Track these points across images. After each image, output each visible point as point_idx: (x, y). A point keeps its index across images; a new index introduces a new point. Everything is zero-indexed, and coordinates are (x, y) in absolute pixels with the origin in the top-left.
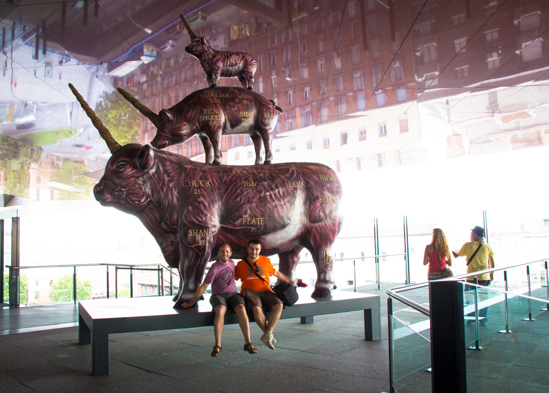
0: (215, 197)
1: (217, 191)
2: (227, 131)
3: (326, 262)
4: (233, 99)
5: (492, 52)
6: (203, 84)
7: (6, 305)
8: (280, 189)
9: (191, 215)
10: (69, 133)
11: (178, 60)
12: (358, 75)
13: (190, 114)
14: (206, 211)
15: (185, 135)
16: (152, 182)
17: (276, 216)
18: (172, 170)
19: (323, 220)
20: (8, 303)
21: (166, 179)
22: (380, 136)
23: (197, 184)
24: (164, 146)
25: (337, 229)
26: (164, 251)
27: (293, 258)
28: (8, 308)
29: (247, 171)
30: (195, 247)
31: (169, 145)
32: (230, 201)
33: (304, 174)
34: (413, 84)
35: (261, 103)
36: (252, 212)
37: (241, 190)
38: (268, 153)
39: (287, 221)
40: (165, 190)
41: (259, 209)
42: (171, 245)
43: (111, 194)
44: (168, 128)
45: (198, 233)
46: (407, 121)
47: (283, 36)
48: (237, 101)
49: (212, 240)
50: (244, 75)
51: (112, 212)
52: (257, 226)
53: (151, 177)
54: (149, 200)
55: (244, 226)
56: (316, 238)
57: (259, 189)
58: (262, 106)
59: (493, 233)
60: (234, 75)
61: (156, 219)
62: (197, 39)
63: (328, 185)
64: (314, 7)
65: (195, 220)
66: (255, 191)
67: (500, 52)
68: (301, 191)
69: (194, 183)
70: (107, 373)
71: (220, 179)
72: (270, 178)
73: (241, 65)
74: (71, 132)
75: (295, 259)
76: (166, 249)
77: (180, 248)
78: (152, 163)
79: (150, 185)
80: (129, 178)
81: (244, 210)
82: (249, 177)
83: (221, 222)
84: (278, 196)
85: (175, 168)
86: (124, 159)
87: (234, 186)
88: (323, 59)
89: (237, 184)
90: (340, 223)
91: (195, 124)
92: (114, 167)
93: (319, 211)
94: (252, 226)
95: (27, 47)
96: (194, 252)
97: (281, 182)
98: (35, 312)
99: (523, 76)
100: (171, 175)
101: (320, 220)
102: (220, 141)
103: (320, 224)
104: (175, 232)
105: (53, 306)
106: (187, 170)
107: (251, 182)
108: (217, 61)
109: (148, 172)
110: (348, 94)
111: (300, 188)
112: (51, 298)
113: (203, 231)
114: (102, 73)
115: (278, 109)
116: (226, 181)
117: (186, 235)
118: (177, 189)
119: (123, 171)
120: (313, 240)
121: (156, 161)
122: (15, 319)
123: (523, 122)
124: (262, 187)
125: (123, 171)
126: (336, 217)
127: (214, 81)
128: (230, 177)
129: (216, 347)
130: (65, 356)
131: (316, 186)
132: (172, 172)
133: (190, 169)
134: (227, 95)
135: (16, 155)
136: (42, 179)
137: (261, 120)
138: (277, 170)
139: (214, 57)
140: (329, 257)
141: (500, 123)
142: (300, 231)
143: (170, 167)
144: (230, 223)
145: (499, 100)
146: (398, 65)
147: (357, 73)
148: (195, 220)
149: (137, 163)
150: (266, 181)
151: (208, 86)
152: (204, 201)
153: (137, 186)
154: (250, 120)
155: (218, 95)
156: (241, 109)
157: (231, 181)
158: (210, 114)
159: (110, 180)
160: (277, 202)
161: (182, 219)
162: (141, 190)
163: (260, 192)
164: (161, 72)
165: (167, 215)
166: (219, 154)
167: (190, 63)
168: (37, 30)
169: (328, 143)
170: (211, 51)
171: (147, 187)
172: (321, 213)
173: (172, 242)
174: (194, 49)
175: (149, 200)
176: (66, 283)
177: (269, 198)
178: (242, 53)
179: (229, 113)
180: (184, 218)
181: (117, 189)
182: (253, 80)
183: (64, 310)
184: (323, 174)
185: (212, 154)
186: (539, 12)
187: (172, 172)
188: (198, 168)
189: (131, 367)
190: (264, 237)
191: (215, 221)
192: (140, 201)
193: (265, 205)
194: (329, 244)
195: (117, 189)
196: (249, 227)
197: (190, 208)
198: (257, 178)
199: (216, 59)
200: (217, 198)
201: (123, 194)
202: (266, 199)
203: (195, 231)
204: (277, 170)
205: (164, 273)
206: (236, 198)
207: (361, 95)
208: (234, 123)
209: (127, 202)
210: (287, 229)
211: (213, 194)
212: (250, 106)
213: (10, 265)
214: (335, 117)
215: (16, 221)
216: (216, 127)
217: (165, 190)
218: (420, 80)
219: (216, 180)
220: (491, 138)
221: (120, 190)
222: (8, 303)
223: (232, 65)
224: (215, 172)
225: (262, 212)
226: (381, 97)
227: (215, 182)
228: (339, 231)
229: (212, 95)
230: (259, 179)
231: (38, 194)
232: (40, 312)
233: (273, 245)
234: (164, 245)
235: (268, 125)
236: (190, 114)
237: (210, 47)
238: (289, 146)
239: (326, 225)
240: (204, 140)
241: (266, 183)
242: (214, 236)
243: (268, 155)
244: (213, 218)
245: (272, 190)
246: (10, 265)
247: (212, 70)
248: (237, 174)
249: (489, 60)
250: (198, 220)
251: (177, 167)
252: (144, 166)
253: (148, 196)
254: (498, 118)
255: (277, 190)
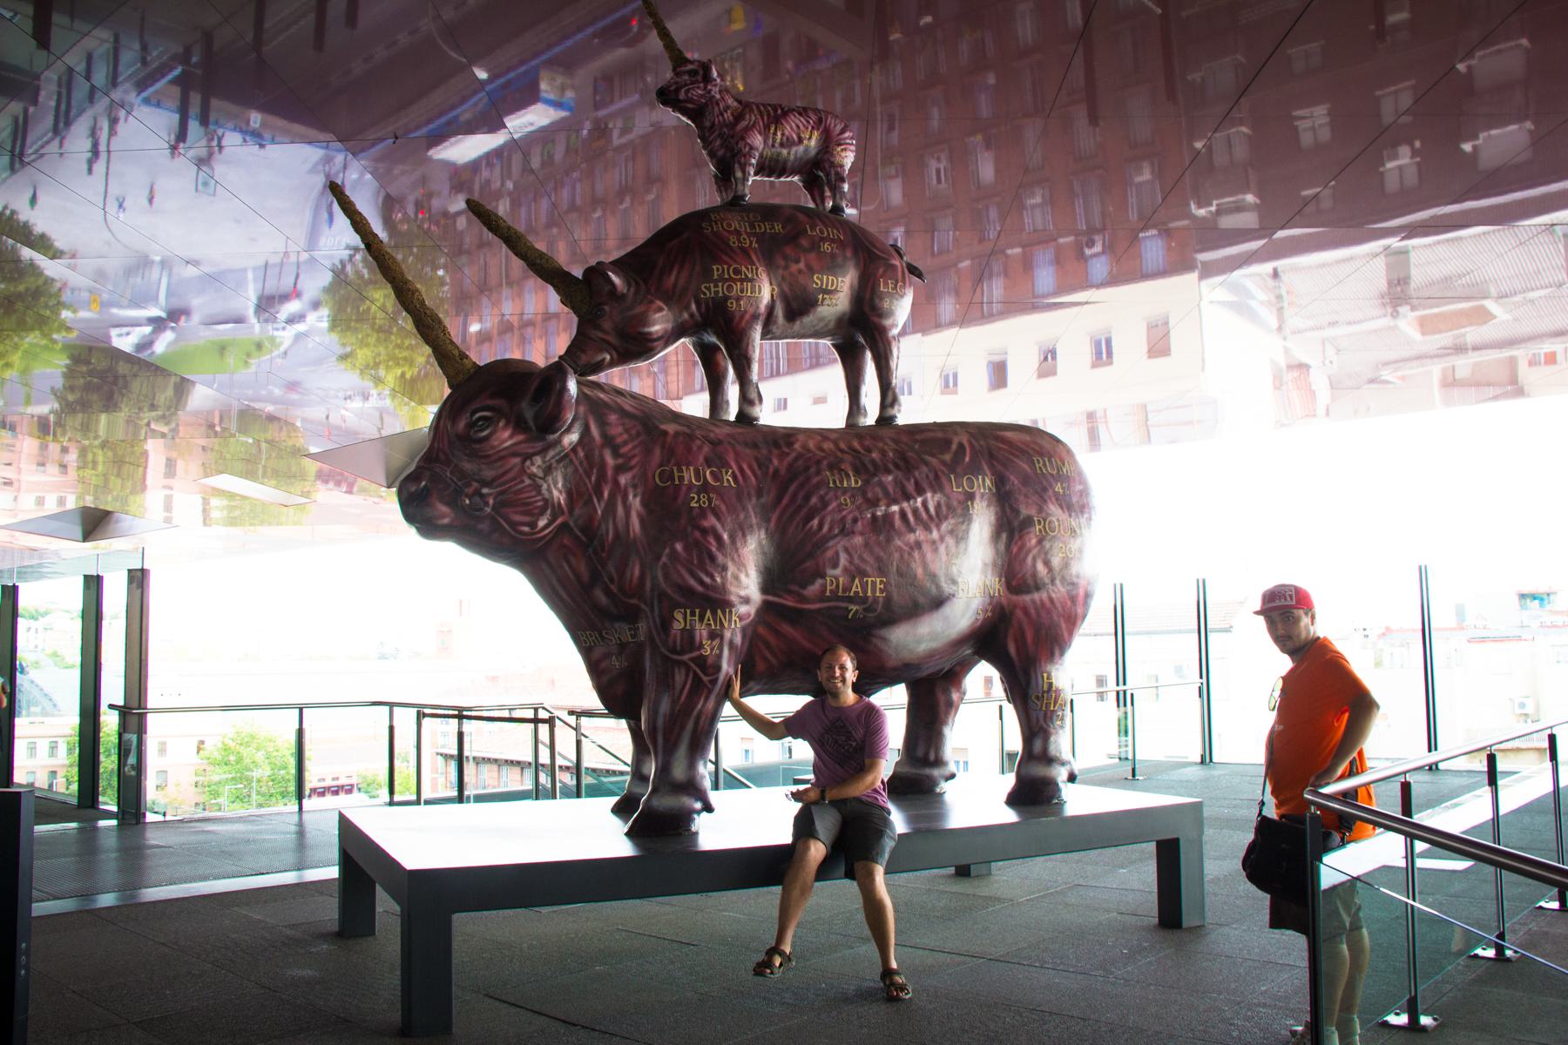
0: (747, 517)
1: (754, 500)
2: (774, 329)
3: (1048, 705)
4: (793, 238)
5: (1395, 145)
6: (706, 196)
7: (108, 815)
8: (929, 495)
9: (679, 567)
10: (253, 348)
11: (551, 156)
12: (1038, 200)
13: (673, 278)
14: (725, 555)
15: (659, 339)
16: (570, 470)
17: (919, 571)
18: (625, 436)
19: (1045, 585)
20: (115, 808)
21: (610, 461)
22: (1094, 366)
23: (698, 479)
24: (598, 367)
25: (1080, 611)
26: (594, 668)
27: (947, 692)
28: (114, 822)
29: (835, 442)
30: (692, 659)
31: (612, 364)
32: (791, 529)
33: (991, 455)
34: (1185, 223)
35: (870, 252)
36: (851, 562)
37: (822, 498)
38: (888, 396)
39: (947, 588)
40: (606, 494)
41: (872, 552)
42: (620, 654)
43: (453, 503)
44: (608, 316)
45: (702, 619)
46: (1166, 323)
47: (838, 96)
48: (804, 243)
49: (738, 640)
50: (818, 174)
51: (451, 555)
52: (864, 600)
53: (566, 456)
54: (559, 521)
55: (829, 599)
56: (1021, 639)
57: (870, 495)
58: (874, 261)
59: (1388, 629)
60: (793, 173)
61: (578, 577)
62: (690, 67)
63: (1058, 488)
64: (920, 15)
65: (692, 582)
66: (860, 501)
67: (1417, 144)
68: (985, 504)
69: (689, 475)
70: (447, 1028)
71: (760, 466)
72: (901, 464)
73: (813, 143)
74: (259, 346)
75: (955, 696)
76: (604, 665)
77: (648, 664)
78: (570, 417)
79: (565, 478)
80: (503, 458)
81: (829, 554)
82: (841, 460)
83: (766, 588)
84: (924, 515)
85: (634, 432)
86: (490, 402)
87: (802, 486)
88: (943, 157)
89: (808, 479)
90: (1088, 596)
91: (687, 307)
92: (461, 425)
93: (1034, 559)
94: (850, 600)
95: (146, 109)
96: (687, 675)
97: (931, 476)
98: (193, 838)
99: (1227, 258)
100: (623, 450)
101: (1038, 588)
102: (756, 355)
103: (1036, 596)
104: (632, 616)
105: (240, 820)
106: (669, 439)
107: (848, 476)
108: (748, 129)
109: (559, 441)
110: (1009, 252)
111: (982, 495)
112: (200, 789)
113: (714, 614)
114: (355, 176)
115: (913, 270)
116: (776, 471)
117: (666, 624)
118: (639, 490)
119: (486, 438)
120: (1016, 641)
121: (582, 409)
122: (134, 854)
123: (1472, 334)
124: (878, 490)
125: (486, 438)
126: (1078, 576)
127: (740, 187)
128: (789, 459)
129: (775, 950)
130: (307, 973)
131: (1024, 490)
132: (625, 443)
133: (677, 434)
134: (778, 227)
135: (110, 404)
136: (180, 465)
137: (872, 299)
138: (916, 441)
139: (738, 117)
140: (1058, 691)
141: (1414, 333)
142: (981, 617)
143: (620, 429)
144: (790, 592)
145: (1414, 272)
146: (1145, 176)
147: (1033, 195)
148: (692, 582)
149: (529, 414)
150: (889, 472)
151: (718, 201)
152: (719, 526)
153: (528, 482)
154: (838, 292)
155: (752, 226)
156: (815, 264)
157: (793, 473)
158: (730, 279)
159: (448, 463)
160: (920, 534)
161: (654, 578)
162: (539, 493)
163: (874, 503)
164: (510, 185)
165: (611, 567)
166: (753, 395)
167: (583, 166)
168: (184, 59)
169: (955, 384)
170: (730, 101)
171: (555, 484)
172: (1040, 567)
173: (622, 646)
174: (682, 96)
175: (559, 521)
176: (242, 749)
177: (898, 522)
178: (816, 111)
179: (783, 278)
180: (660, 575)
181: (470, 490)
182: (846, 187)
183: (274, 832)
184: (1041, 454)
185: (732, 392)
186: (1524, 42)
187: (625, 443)
188: (698, 433)
189: (513, 1010)
190: (884, 632)
191: (746, 583)
192: (533, 525)
193: (889, 540)
194: (1057, 653)
195: (470, 490)
196: (843, 605)
197: (679, 547)
198: (863, 464)
199: (744, 124)
200: (754, 521)
201: (487, 504)
202: (892, 524)
203: (693, 614)
204: (916, 441)
205: (557, 730)
206: (809, 518)
207: (1043, 256)
208: (794, 305)
209: (497, 527)
210: (947, 610)
211: (744, 508)
212: (839, 260)
213: (121, 703)
214: (973, 313)
215: (138, 579)
216: (747, 317)
217: (606, 494)
218: (1202, 212)
219: (751, 468)
220: (1386, 374)
221: (478, 493)
222: (115, 808)
223: (788, 143)
224: (746, 444)
225: (878, 559)
226: (1153, 248)
227: (748, 472)
228: (1084, 617)
229: (735, 225)
230: (871, 468)
231: (168, 507)
232: (209, 837)
233: (906, 656)
234: (598, 653)
235: (890, 314)
236: (673, 278)
237: (727, 91)
238: (944, 373)
239: (1051, 600)
240: (708, 356)
241: (890, 478)
242: (744, 630)
243: (889, 399)
244: (742, 577)
245: (908, 497)
246: (121, 703)
247: (734, 156)
248: (809, 450)
249: (1389, 165)
250: (702, 583)
251: (639, 428)
252: (549, 424)
253: (557, 511)
254: (1407, 322)
255: (919, 500)
